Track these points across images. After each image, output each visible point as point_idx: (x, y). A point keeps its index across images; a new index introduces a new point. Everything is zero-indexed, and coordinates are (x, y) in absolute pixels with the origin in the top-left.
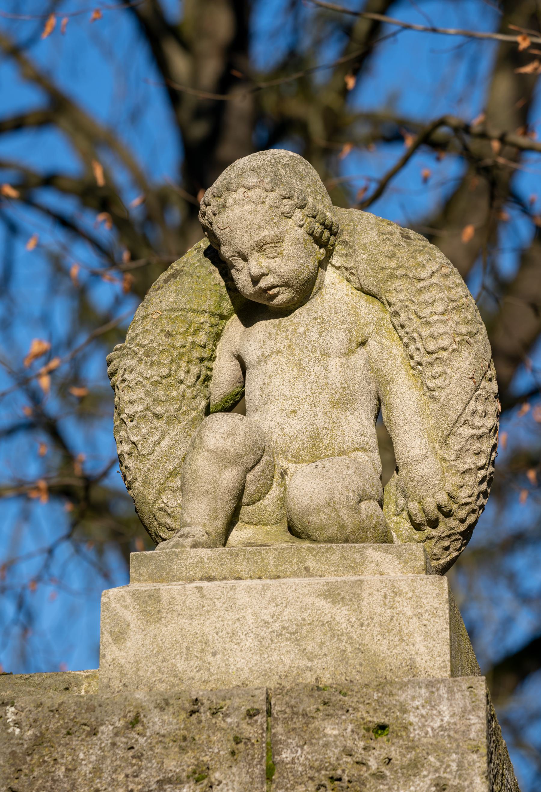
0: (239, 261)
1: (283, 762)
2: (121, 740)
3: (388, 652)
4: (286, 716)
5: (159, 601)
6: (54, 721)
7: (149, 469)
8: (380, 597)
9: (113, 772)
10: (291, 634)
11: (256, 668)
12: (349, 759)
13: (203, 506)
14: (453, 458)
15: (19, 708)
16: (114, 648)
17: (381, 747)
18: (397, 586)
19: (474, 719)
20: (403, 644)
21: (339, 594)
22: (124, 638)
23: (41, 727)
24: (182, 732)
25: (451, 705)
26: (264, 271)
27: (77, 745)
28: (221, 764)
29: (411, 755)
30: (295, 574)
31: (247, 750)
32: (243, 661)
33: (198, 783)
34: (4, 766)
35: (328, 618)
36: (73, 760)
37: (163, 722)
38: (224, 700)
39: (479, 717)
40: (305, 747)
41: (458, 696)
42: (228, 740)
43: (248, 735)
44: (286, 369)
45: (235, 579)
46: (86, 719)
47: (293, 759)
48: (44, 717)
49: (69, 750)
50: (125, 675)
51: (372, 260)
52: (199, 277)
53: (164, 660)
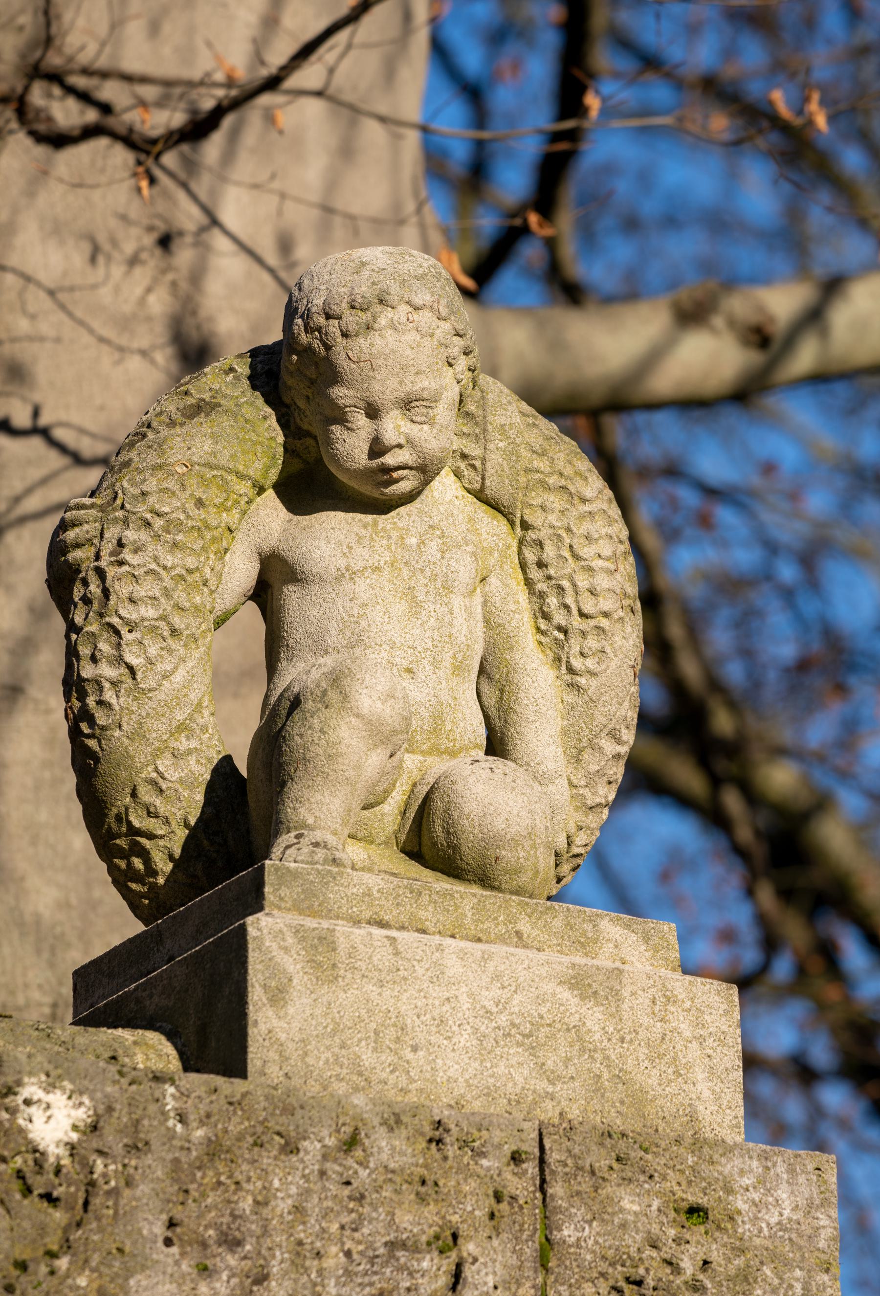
0: (360, 416)
1: (564, 1242)
2: (332, 1168)
3: (659, 1089)
4: (567, 1170)
5: (334, 950)
6: (235, 1120)
7: (148, 714)
8: (647, 1001)
9: (323, 1217)
10: (524, 1036)
11: (476, 1082)
12: (654, 1254)
13: (337, 802)
14: (583, 783)
15: (183, 1090)
16: (270, 1013)
17: (698, 1242)
18: (669, 987)
19: (824, 1221)
20: (680, 1080)
21: (589, 985)
22: (284, 999)
23: (216, 1126)
24: (419, 1169)
25: (792, 1192)
26: (402, 441)
27: (269, 1164)
28: (476, 1230)
29: (739, 1262)
30: (502, 939)
31: (513, 1214)
32: (456, 1067)
33: (444, 1256)
34: (163, 1181)
35: (573, 1021)
36: (264, 1188)
37: (393, 1148)
38: (479, 1130)
39: (830, 1217)
40: (595, 1224)
41: (802, 1179)
42: (488, 1195)
43: (514, 1192)
44: (391, 599)
45: (418, 931)
46: (282, 1125)
47: (578, 1239)
48: (220, 1110)
49: (258, 1171)
50: (287, 1059)
51: (512, 454)
52: (247, 421)
53: (343, 1046)
